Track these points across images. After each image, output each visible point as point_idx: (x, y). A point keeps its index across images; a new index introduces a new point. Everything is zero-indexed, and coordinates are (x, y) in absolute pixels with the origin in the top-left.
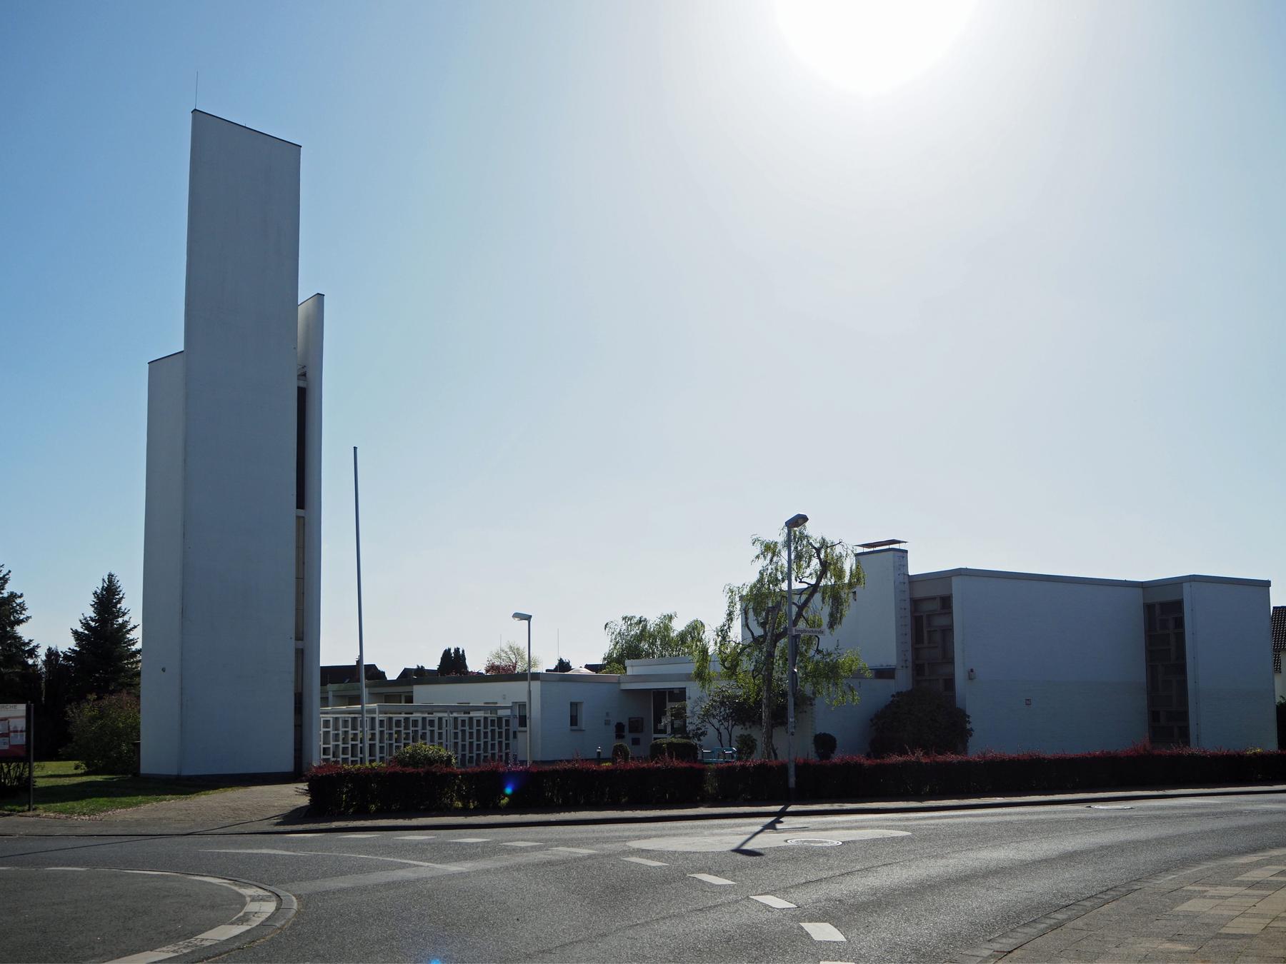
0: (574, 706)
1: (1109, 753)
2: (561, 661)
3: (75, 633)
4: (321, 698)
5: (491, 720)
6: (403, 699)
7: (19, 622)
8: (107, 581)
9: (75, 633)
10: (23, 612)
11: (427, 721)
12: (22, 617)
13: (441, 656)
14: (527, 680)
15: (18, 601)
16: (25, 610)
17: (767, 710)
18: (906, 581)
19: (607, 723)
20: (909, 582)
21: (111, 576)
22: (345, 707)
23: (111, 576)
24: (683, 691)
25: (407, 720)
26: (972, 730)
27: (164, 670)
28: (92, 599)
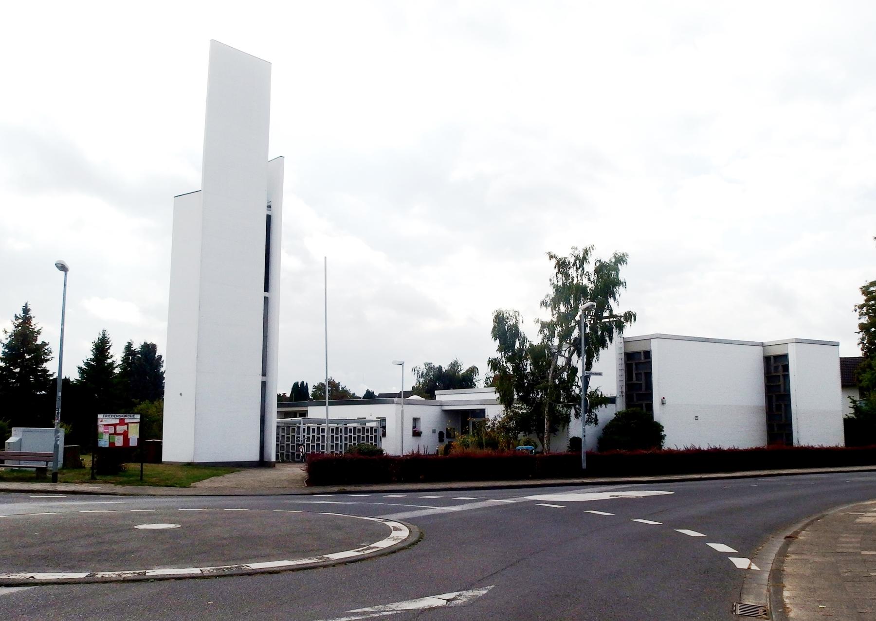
0: (416, 420)
1: (812, 446)
2: (368, 392)
3: (80, 368)
4: (277, 412)
5: (358, 429)
6: (298, 415)
7: (47, 361)
8: (102, 334)
9: (80, 368)
10: (50, 354)
11: (348, 430)
12: (48, 357)
13: (292, 387)
14: (325, 405)
15: (46, 347)
16: (51, 353)
17: (548, 423)
18: (622, 341)
19: (434, 431)
20: (624, 342)
21: (104, 331)
22: (290, 419)
23: (104, 331)
24: (483, 411)
25: (337, 428)
26: (665, 435)
27: (181, 395)
28: (92, 346)
